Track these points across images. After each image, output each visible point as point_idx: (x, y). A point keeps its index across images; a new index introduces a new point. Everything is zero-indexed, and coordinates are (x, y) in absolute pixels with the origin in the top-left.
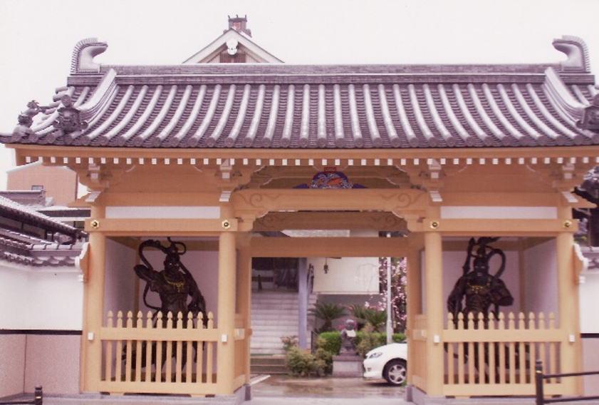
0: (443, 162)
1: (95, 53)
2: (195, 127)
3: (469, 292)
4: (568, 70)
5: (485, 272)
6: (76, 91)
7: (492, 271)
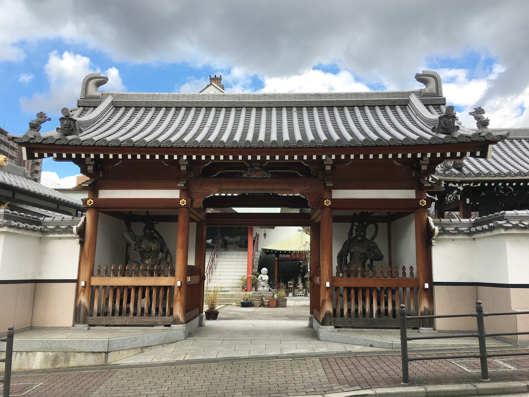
0: (333, 157)
1: (98, 84)
2: (185, 134)
3: (352, 251)
4: (426, 95)
5: (364, 238)
6: (167, 110)
7: (368, 237)
